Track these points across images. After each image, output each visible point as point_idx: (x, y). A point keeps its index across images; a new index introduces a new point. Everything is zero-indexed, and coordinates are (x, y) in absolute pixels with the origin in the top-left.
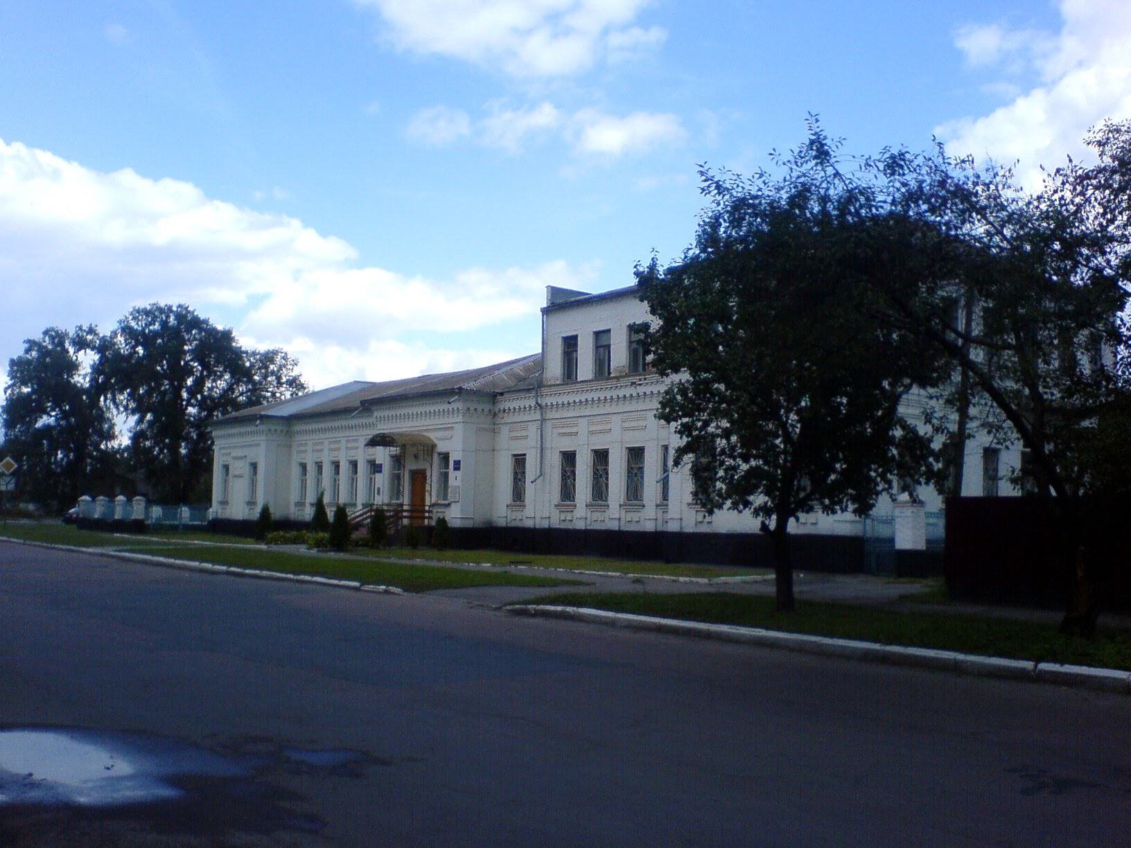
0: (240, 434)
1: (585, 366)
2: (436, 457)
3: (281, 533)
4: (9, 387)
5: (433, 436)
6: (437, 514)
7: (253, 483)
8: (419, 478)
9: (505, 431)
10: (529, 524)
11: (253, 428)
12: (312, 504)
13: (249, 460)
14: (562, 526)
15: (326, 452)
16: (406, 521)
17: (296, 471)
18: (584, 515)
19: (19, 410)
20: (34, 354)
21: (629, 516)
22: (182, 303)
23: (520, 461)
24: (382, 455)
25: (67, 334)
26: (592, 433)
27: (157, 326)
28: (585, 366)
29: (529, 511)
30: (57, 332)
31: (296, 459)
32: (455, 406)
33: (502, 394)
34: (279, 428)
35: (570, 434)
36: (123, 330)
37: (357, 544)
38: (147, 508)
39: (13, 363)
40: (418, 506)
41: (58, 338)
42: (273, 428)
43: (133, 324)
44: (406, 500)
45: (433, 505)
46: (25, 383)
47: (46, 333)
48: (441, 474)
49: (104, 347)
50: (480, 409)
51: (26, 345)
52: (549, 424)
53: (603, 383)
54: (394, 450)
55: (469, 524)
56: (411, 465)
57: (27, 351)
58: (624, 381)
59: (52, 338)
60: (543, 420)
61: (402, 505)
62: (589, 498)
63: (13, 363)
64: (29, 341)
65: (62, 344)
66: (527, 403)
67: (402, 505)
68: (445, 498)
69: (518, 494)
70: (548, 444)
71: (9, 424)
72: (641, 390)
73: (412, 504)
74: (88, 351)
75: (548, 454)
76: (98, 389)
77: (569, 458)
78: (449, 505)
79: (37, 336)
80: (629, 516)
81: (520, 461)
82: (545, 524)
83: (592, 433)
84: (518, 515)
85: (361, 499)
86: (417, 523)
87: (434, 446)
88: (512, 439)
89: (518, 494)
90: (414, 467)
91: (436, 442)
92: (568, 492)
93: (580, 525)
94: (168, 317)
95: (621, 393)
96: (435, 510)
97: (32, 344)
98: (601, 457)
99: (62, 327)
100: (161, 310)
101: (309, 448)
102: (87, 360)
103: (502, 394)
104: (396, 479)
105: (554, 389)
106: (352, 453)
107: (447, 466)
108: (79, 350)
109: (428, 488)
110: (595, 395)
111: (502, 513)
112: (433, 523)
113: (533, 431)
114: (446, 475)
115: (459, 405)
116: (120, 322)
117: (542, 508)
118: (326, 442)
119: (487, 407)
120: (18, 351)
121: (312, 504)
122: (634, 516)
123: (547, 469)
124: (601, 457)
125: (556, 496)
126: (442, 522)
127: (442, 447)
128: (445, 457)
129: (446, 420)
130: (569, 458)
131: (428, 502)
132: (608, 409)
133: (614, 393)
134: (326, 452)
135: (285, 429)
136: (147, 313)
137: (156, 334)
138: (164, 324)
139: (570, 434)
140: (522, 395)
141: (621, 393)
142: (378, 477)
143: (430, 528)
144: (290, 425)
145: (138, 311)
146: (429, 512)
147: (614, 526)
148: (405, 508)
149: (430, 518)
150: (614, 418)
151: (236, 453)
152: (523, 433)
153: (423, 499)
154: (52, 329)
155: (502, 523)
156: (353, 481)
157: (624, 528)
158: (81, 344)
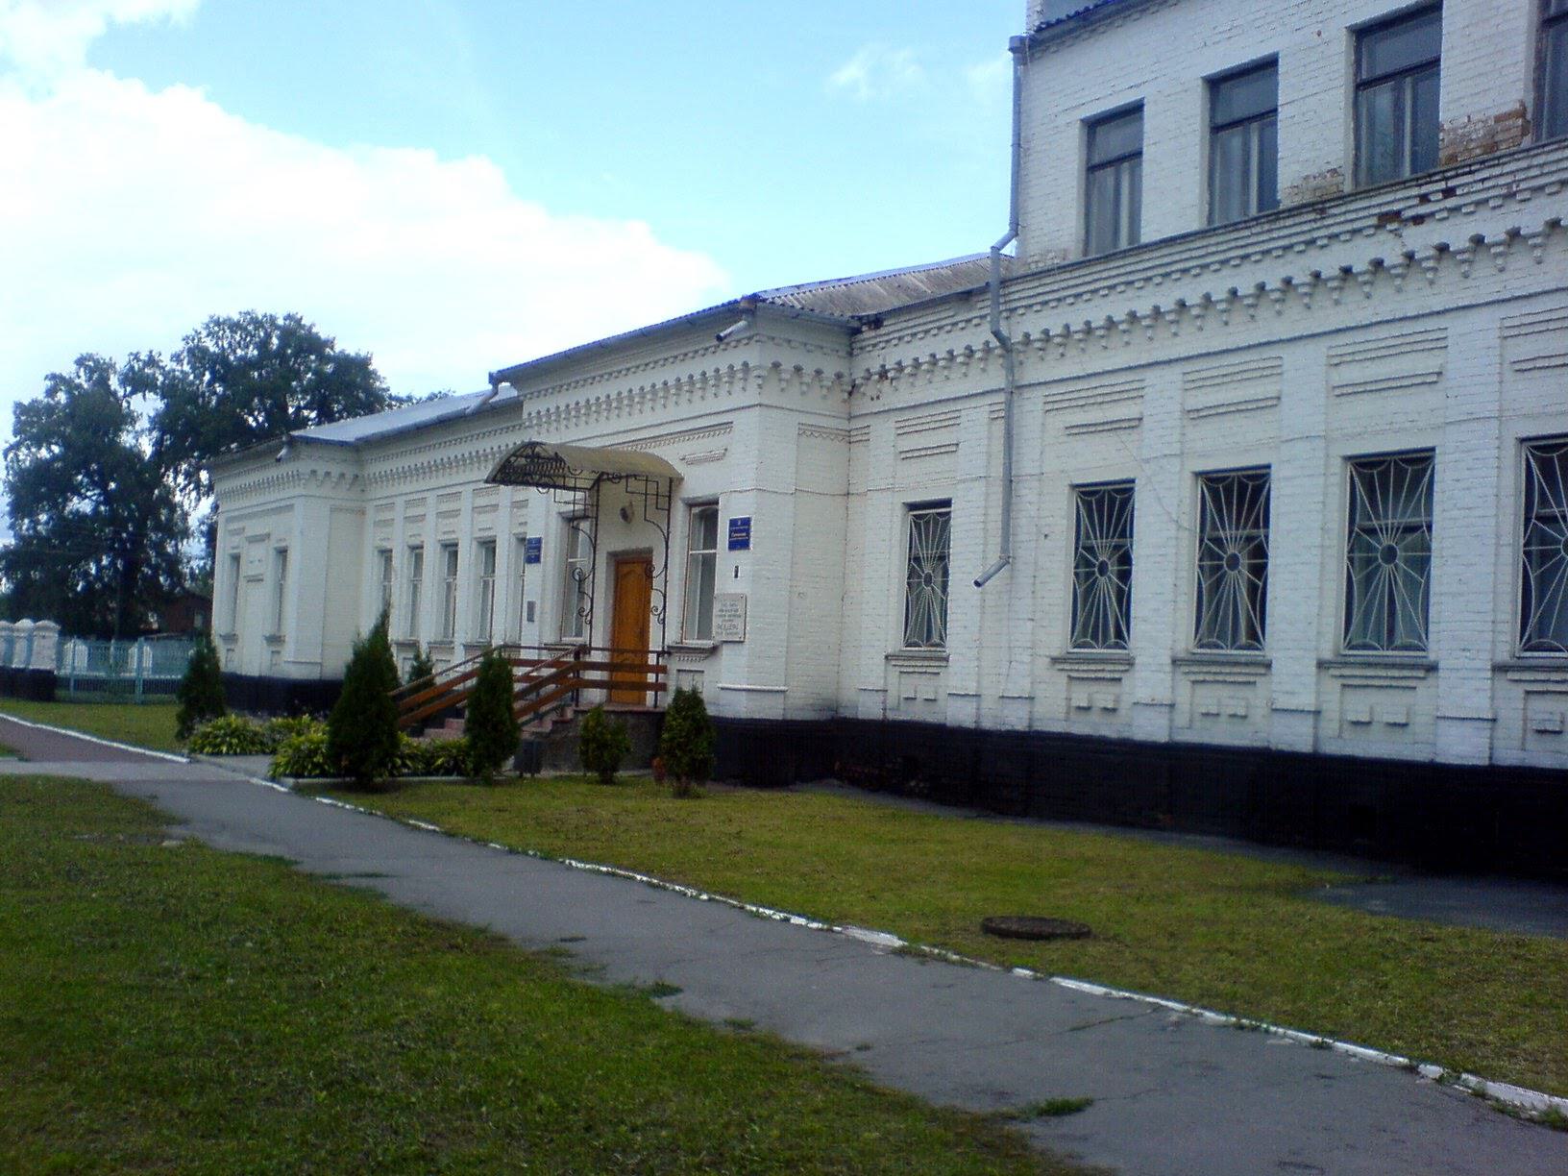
0: (258, 488)
1: (1172, 190)
2: (680, 516)
3: (234, 719)
4: (11, 448)
5: (671, 454)
6: (678, 679)
7: (280, 589)
8: (633, 573)
9: (883, 432)
10: (959, 714)
11: (273, 472)
12: (468, 647)
13: (273, 544)
14: (1081, 727)
15: (431, 518)
16: (594, 696)
17: (372, 566)
18: (1163, 695)
19: (34, 489)
20: (62, 397)
21: (1359, 705)
22: (293, 312)
23: (929, 521)
24: (542, 510)
25: (112, 366)
26: (1196, 415)
27: (253, 352)
28: (1172, 190)
29: (289, 652)
30: (96, 362)
31: (373, 539)
32: (736, 357)
33: (876, 322)
34: (335, 470)
35: (1113, 427)
36: (190, 351)
37: (428, 764)
38: (60, 645)
39: (20, 409)
40: (629, 659)
41: (98, 370)
42: (322, 468)
43: (210, 345)
44: (598, 636)
45: (666, 652)
46: (39, 441)
47: (80, 362)
48: (692, 560)
49: (172, 390)
50: (809, 370)
51: (49, 383)
52: (1032, 405)
53: (1259, 237)
54: (566, 500)
55: (770, 710)
56: (616, 540)
57: (51, 392)
58: (1340, 218)
59: (91, 371)
60: (1015, 389)
61: (584, 649)
62: (1183, 637)
63: (20, 409)
64: (53, 377)
65: (103, 382)
66: (958, 341)
67: (584, 649)
68: (704, 631)
69: (924, 626)
70: (1028, 463)
71: (21, 507)
72: (1420, 239)
73: (614, 649)
74: (150, 395)
75: (1027, 493)
76: (165, 457)
77: (1106, 509)
78: (714, 650)
79: (68, 369)
80: (1359, 705)
81: (929, 521)
82: (1015, 719)
83: (1196, 415)
84: (924, 687)
85: (465, 631)
86: (626, 702)
87: (674, 482)
88: (907, 456)
89: (924, 626)
90: (619, 546)
91: (681, 468)
92: (1101, 613)
93: (1151, 729)
94: (268, 336)
95: (1329, 262)
96: (674, 664)
97: (57, 381)
98: (1237, 498)
99: (104, 354)
100: (258, 323)
101: (398, 513)
102: (147, 406)
103: (876, 322)
104: (575, 583)
105: (1051, 284)
106: (485, 520)
107: (711, 540)
108: (133, 392)
109: (656, 600)
110: (1217, 285)
111: (872, 682)
112: (667, 700)
113: (977, 429)
114: (708, 565)
115: (752, 355)
116: (186, 339)
117: (1005, 668)
118: (431, 497)
119: (831, 366)
120: (34, 391)
121: (468, 647)
122: (924, 687)
123: (1025, 551)
124: (1237, 498)
125: (1057, 635)
126: (690, 703)
127: (697, 484)
128: (706, 513)
129: (712, 404)
130: (1106, 509)
131: (655, 643)
132: (1270, 325)
133: (1299, 268)
134: (431, 518)
135: (350, 473)
136: (235, 326)
137: (247, 364)
138: (263, 346)
139: (1113, 427)
140: (945, 315)
141: (1329, 262)
142: (533, 572)
143: (657, 718)
144: (360, 463)
145: (218, 323)
146: (660, 669)
147: (1294, 737)
148: (597, 657)
149: (660, 687)
150: (1291, 356)
151: (255, 528)
152: (944, 437)
153: (643, 634)
154: (90, 357)
155: (869, 709)
156: (487, 587)
157: (1331, 748)
158: (138, 381)
